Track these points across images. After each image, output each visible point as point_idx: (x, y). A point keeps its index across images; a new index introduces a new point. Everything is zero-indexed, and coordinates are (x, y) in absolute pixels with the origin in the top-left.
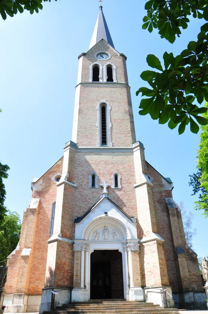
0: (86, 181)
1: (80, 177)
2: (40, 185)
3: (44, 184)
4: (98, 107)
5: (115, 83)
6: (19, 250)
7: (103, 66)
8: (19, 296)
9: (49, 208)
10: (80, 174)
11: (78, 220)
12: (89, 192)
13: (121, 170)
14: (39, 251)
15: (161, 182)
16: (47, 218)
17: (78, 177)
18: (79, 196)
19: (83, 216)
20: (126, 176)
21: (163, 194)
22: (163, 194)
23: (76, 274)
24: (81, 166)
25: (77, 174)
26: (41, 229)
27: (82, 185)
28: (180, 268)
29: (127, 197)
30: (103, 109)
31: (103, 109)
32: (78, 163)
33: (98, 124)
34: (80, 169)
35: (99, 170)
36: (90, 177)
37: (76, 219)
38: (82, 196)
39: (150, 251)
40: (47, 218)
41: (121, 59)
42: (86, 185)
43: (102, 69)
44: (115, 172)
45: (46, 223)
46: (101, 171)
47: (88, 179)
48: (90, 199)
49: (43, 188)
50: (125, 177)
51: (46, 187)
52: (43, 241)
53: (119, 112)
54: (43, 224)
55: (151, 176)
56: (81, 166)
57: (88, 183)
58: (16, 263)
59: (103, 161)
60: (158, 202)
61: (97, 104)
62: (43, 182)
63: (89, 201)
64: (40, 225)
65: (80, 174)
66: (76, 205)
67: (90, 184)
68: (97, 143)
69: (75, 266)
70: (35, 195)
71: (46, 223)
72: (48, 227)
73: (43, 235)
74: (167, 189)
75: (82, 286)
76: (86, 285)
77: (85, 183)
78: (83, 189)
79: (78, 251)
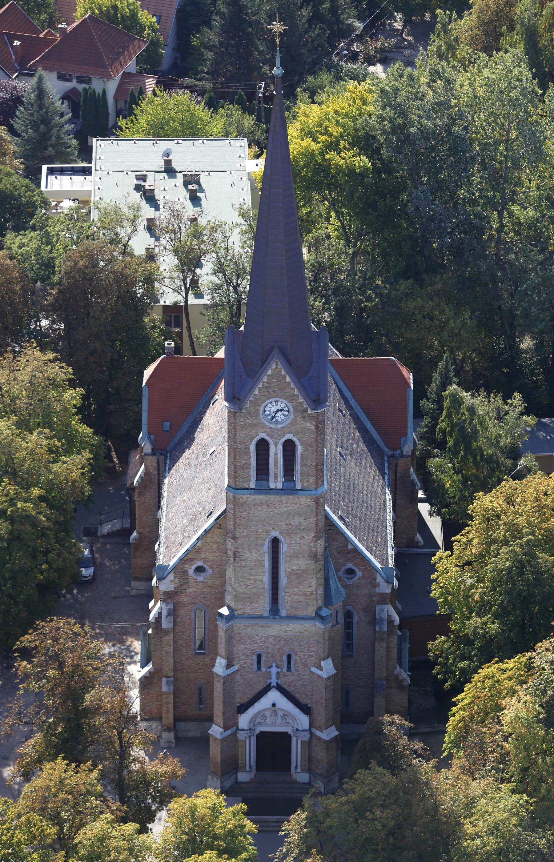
0: (249, 662)
1: (242, 658)
2: (171, 581)
3: (177, 580)
4: (266, 546)
5: (283, 618)
7: (276, 444)
10: (241, 654)
11: (243, 708)
12: (253, 675)
13: (296, 649)
15: (375, 579)
17: (239, 657)
18: (242, 680)
19: (248, 702)
20: (302, 657)
21: (375, 599)
22: (375, 599)
24: (242, 643)
25: (238, 654)
27: (244, 668)
28: (375, 709)
29: (301, 683)
30: (275, 542)
31: (275, 542)
32: (238, 639)
33: (267, 579)
34: (241, 647)
35: (267, 648)
36: (255, 658)
38: (245, 680)
41: (314, 423)
42: (249, 668)
43: (276, 454)
44: (287, 651)
45: (189, 637)
46: (270, 650)
47: (252, 660)
48: (255, 683)
49: (176, 585)
50: (301, 658)
51: (181, 585)
53: (301, 556)
55: (359, 569)
56: (242, 643)
57: (252, 665)
59: (272, 636)
60: (363, 610)
61: (264, 540)
62: (175, 577)
63: (254, 686)
65: (241, 654)
67: (255, 667)
68: (264, 607)
74: (382, 592)
75: (248, 768)
76: (252, 764)
77: (248, 664)
78: (247, 672)
79: (242, 740)
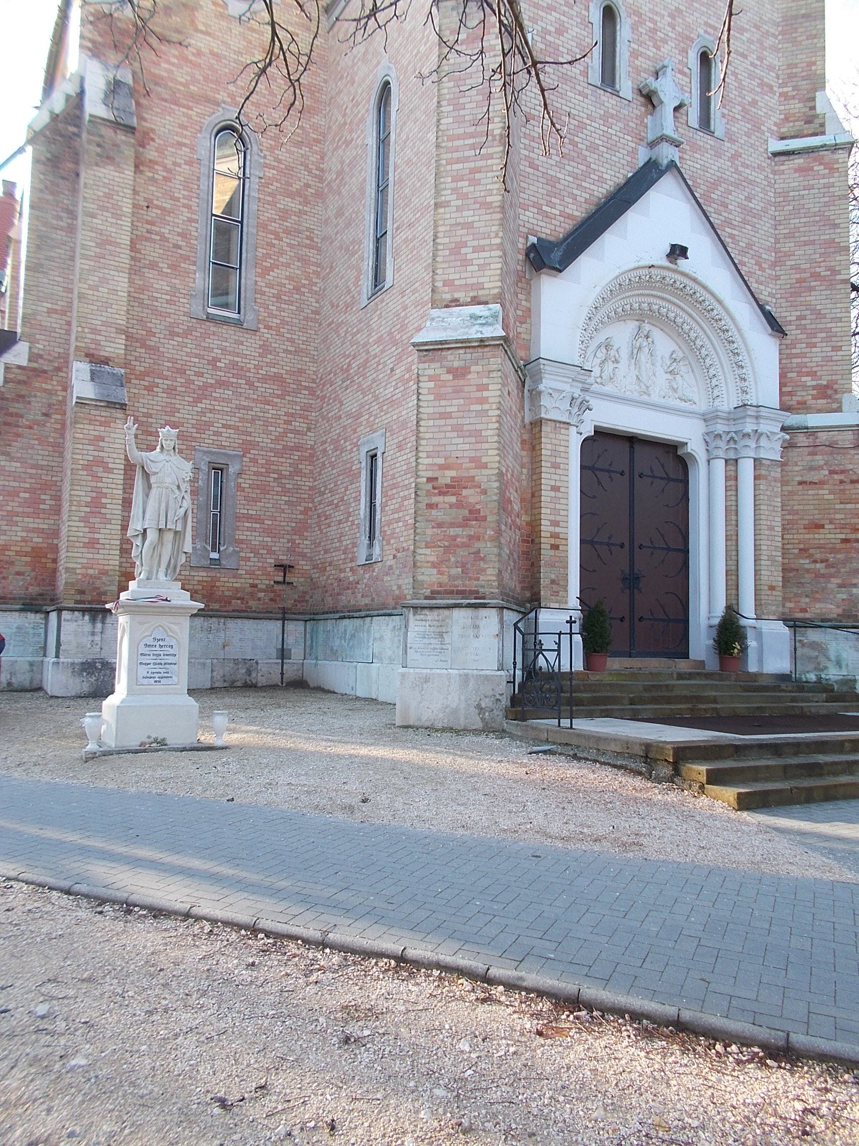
6: (24, 363)
8: (93, 620)
9: (193, 149)
14: (149, 389)
16: (184, 206)
23: (552, 541)
26: (153, 266)
37: (533, 245)
39: (832, 472)
40: (184, 206)
48: (593, 148)
52: (173, 334)
54: (164, 239)
58: (18, 435)
64: (147, 239)
66: (532, 165)
69: (546, 495)
70: (99, 39)
71: (183, 235)
72: (194, 264)
73: (168, 302)
